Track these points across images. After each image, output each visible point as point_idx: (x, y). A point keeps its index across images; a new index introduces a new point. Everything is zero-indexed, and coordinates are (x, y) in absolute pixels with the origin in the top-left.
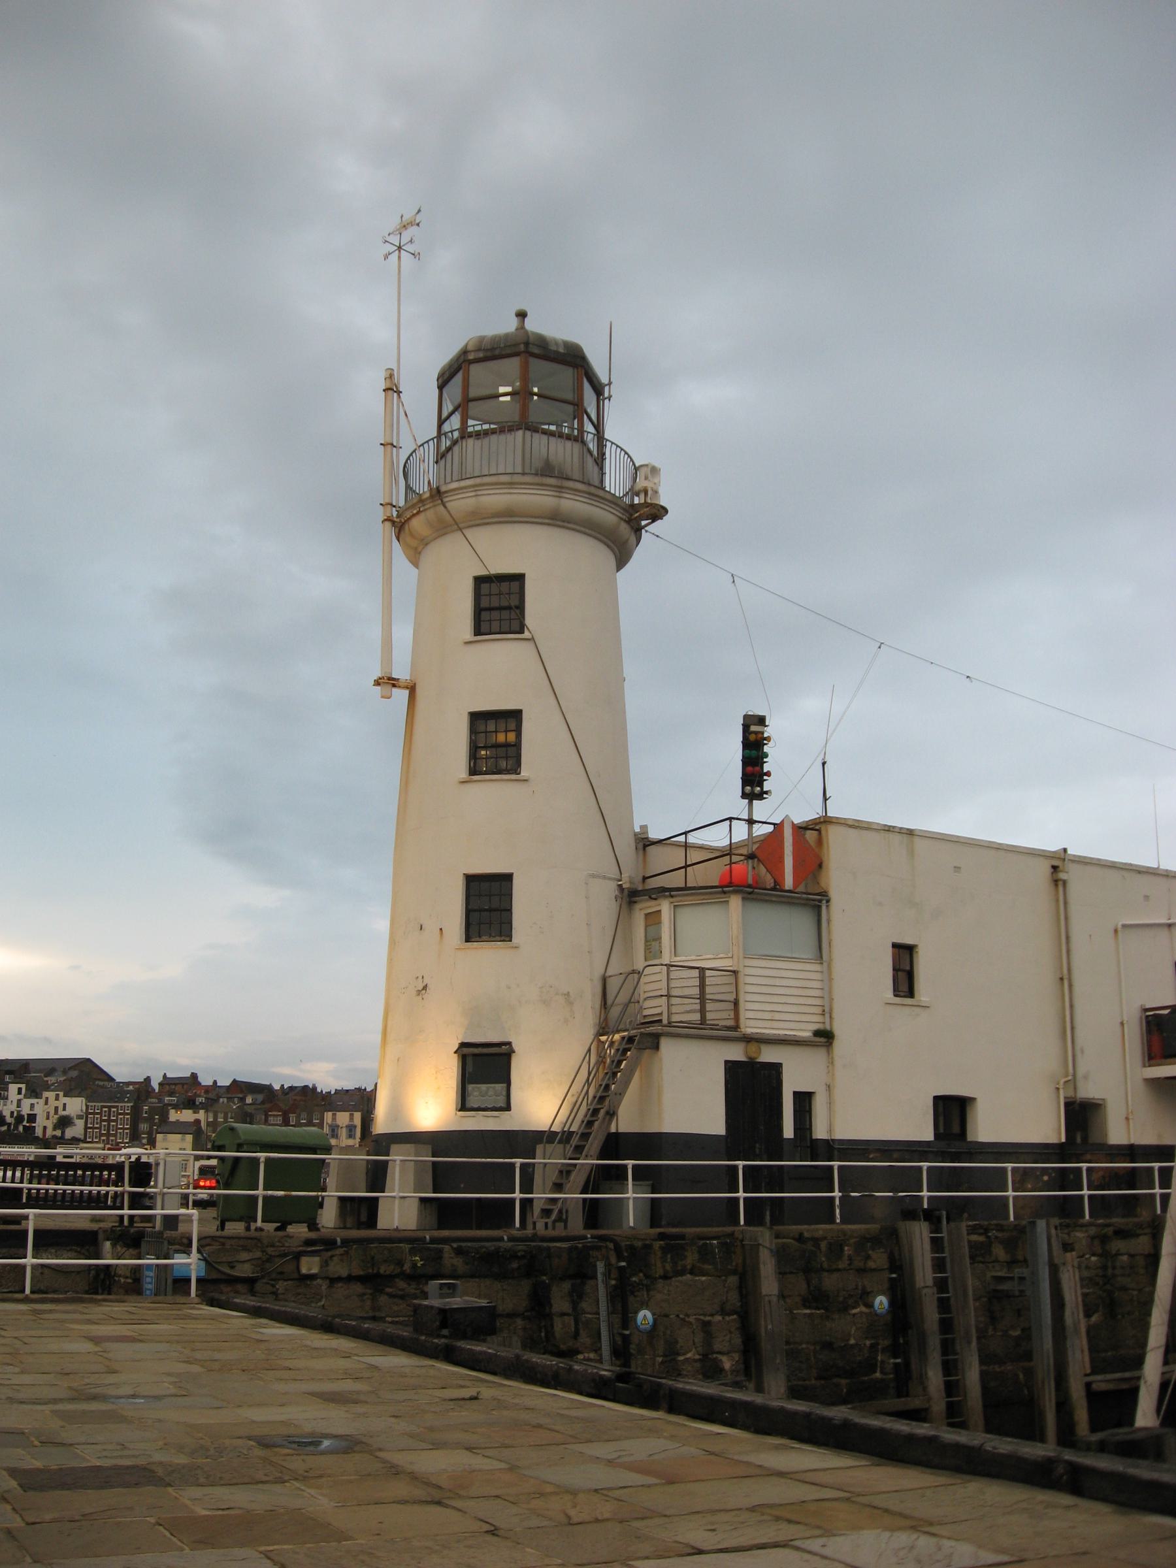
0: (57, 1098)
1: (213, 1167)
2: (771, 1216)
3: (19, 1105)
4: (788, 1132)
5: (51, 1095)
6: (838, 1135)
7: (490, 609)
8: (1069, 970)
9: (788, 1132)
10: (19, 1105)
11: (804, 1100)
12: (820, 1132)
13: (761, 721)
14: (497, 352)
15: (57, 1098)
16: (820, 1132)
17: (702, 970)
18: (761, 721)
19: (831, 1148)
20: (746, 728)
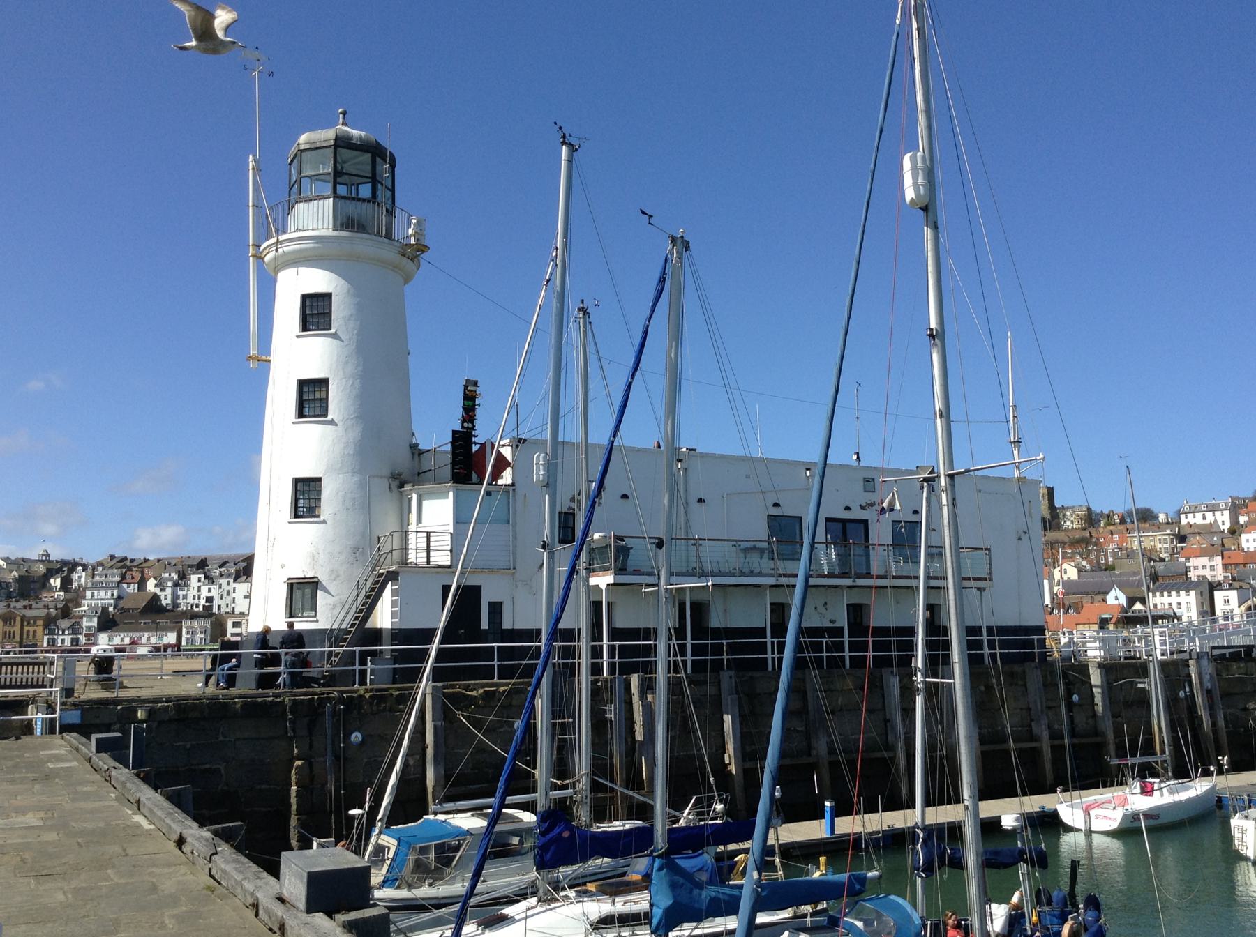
0: (228, 583)
1: (642, 680)
2: (1093, 704)
3: (199, 590)
4: (485, 625)
5: (224, 582)
6: (516, 627)
7: (312, 315)
8: (687, 523)
9: (485, 625)
10: (199, 590)
11: (496, 608)
12: (507, 625)
13: (475, 383)
14: (318, 145)
15: (228, 583)
16: (507, 625)
17: (428, 533)
18: (475, 383)
19: (717, 633)
20: (466, 387)
